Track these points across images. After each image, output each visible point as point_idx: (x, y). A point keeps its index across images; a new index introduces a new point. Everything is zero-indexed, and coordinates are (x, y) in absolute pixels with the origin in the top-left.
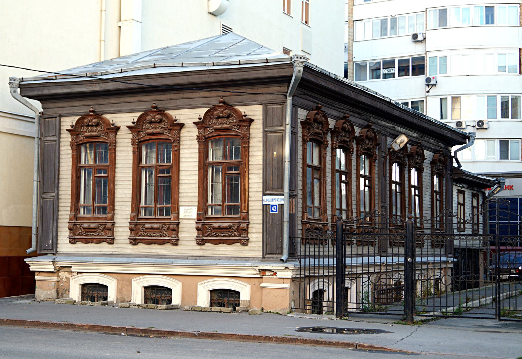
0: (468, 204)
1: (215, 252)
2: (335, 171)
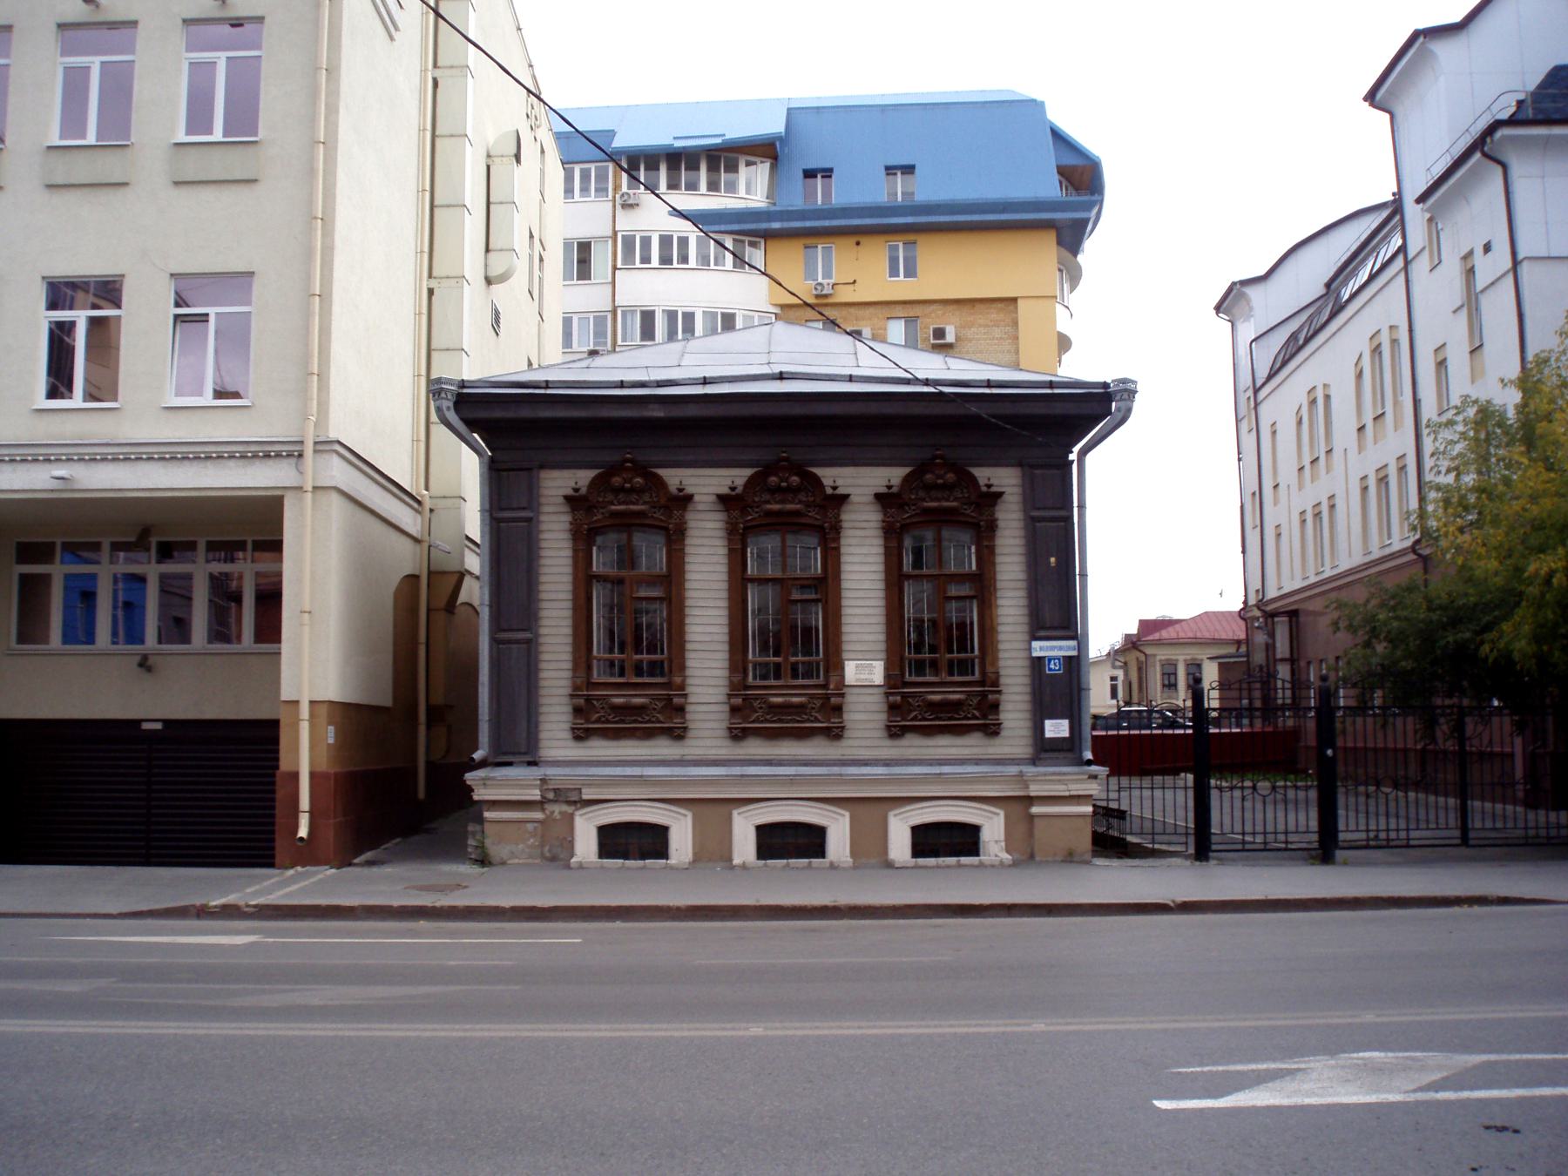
0: (1012, 611)
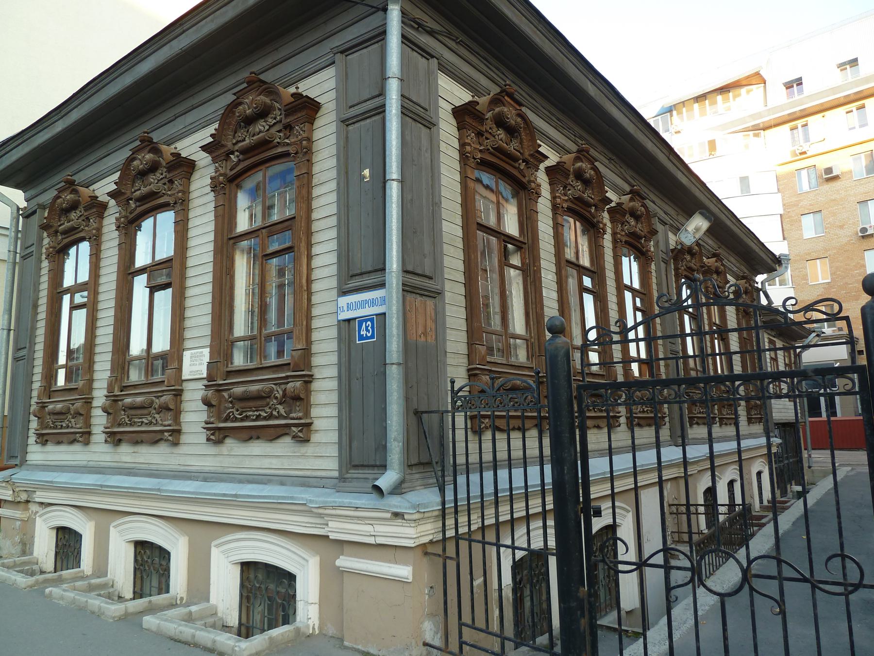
1: (247, 463)
2: (563, 263)
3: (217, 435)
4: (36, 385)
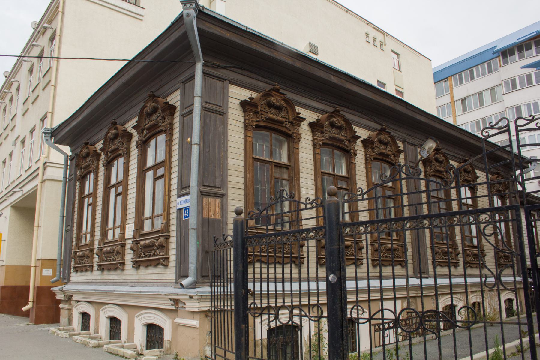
3: (137, 265)
4: (74, 243)
